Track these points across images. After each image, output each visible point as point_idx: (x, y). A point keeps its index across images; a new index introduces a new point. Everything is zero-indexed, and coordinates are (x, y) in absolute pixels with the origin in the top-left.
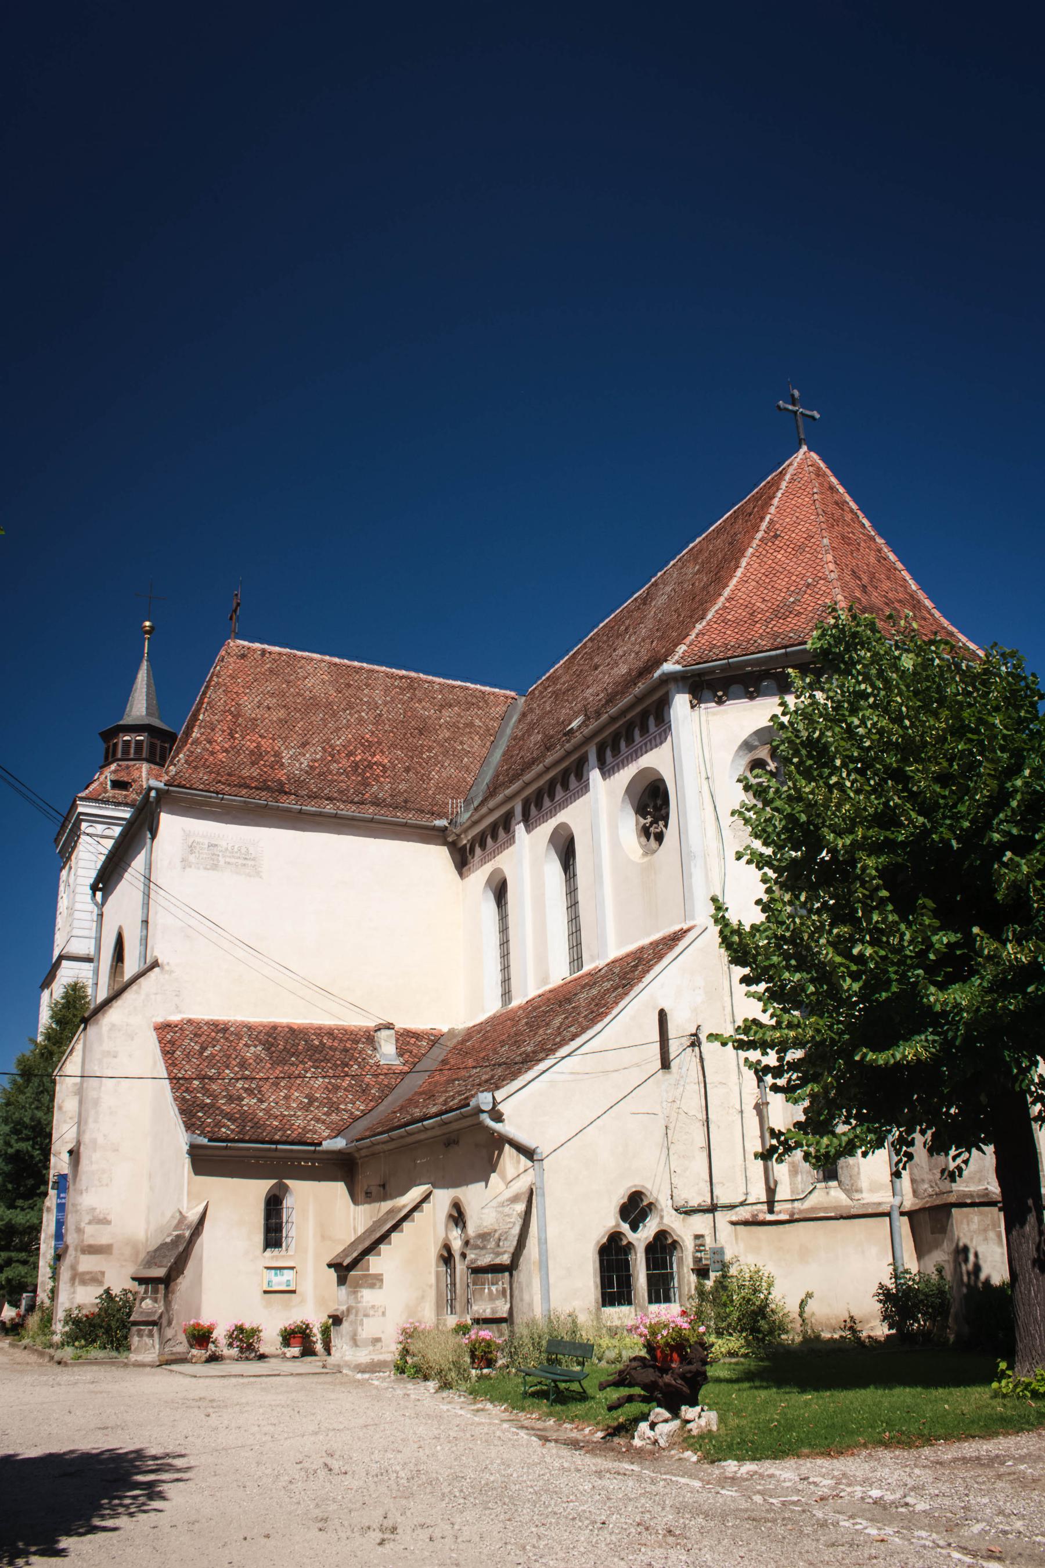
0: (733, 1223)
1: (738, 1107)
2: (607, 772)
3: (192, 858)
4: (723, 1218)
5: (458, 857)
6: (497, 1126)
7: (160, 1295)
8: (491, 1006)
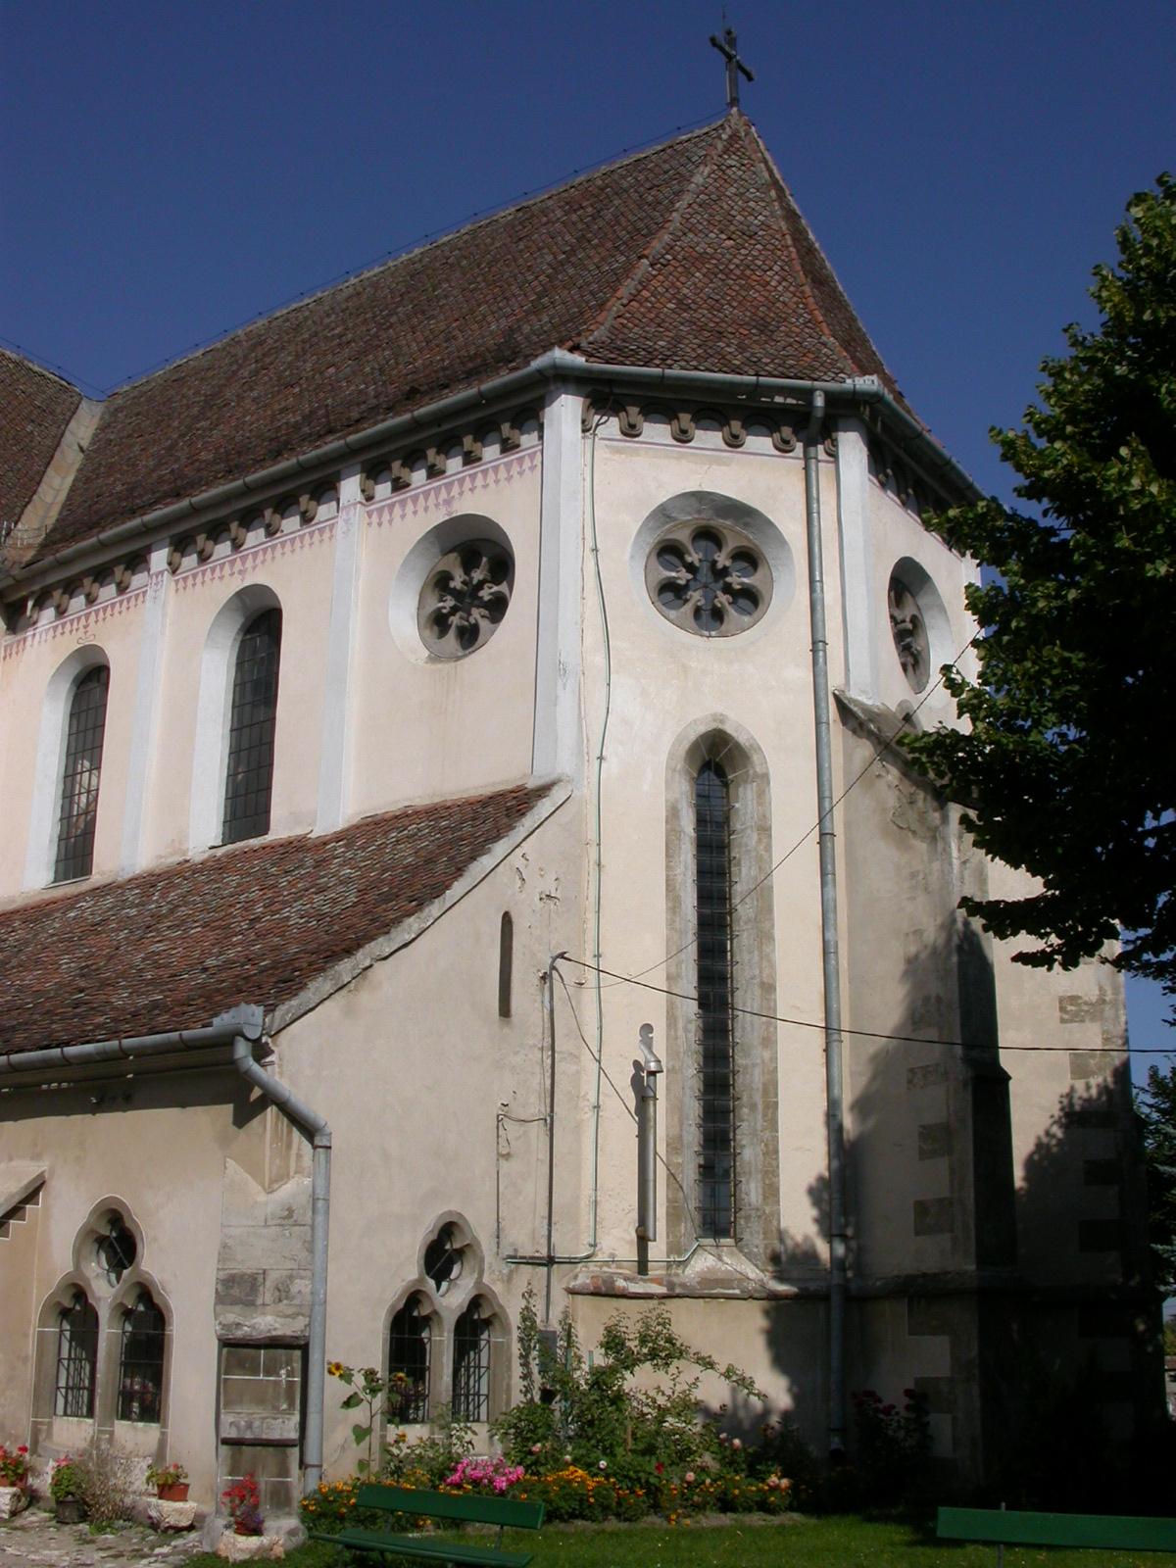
1: (593, 1100)
4: (561, 1278)
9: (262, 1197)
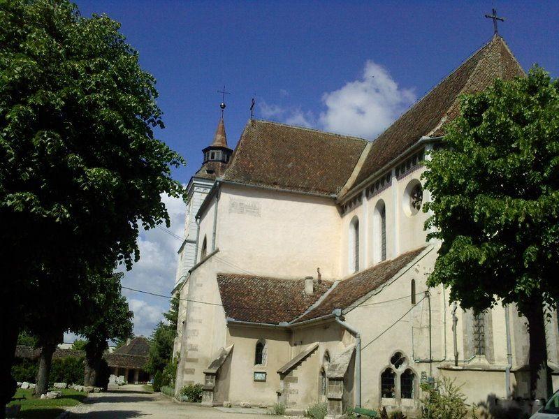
0: (439, 368)
2: (398, 178)
3: (233, 209)
4: (435, 366)
5: (340, 210)
6: (343, 323)
7: (214, 380)
8: (351, 272)
9: (344, 348)
